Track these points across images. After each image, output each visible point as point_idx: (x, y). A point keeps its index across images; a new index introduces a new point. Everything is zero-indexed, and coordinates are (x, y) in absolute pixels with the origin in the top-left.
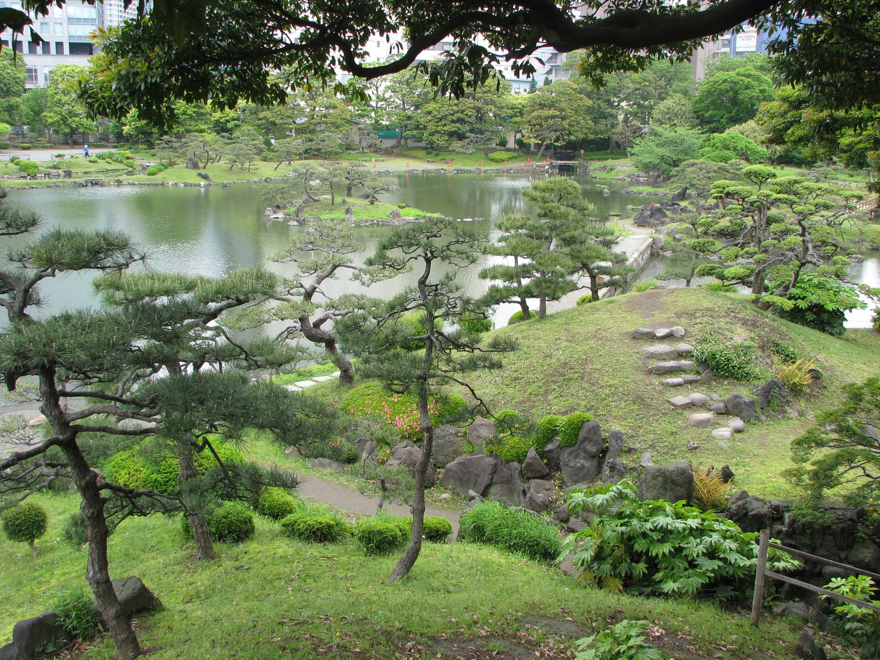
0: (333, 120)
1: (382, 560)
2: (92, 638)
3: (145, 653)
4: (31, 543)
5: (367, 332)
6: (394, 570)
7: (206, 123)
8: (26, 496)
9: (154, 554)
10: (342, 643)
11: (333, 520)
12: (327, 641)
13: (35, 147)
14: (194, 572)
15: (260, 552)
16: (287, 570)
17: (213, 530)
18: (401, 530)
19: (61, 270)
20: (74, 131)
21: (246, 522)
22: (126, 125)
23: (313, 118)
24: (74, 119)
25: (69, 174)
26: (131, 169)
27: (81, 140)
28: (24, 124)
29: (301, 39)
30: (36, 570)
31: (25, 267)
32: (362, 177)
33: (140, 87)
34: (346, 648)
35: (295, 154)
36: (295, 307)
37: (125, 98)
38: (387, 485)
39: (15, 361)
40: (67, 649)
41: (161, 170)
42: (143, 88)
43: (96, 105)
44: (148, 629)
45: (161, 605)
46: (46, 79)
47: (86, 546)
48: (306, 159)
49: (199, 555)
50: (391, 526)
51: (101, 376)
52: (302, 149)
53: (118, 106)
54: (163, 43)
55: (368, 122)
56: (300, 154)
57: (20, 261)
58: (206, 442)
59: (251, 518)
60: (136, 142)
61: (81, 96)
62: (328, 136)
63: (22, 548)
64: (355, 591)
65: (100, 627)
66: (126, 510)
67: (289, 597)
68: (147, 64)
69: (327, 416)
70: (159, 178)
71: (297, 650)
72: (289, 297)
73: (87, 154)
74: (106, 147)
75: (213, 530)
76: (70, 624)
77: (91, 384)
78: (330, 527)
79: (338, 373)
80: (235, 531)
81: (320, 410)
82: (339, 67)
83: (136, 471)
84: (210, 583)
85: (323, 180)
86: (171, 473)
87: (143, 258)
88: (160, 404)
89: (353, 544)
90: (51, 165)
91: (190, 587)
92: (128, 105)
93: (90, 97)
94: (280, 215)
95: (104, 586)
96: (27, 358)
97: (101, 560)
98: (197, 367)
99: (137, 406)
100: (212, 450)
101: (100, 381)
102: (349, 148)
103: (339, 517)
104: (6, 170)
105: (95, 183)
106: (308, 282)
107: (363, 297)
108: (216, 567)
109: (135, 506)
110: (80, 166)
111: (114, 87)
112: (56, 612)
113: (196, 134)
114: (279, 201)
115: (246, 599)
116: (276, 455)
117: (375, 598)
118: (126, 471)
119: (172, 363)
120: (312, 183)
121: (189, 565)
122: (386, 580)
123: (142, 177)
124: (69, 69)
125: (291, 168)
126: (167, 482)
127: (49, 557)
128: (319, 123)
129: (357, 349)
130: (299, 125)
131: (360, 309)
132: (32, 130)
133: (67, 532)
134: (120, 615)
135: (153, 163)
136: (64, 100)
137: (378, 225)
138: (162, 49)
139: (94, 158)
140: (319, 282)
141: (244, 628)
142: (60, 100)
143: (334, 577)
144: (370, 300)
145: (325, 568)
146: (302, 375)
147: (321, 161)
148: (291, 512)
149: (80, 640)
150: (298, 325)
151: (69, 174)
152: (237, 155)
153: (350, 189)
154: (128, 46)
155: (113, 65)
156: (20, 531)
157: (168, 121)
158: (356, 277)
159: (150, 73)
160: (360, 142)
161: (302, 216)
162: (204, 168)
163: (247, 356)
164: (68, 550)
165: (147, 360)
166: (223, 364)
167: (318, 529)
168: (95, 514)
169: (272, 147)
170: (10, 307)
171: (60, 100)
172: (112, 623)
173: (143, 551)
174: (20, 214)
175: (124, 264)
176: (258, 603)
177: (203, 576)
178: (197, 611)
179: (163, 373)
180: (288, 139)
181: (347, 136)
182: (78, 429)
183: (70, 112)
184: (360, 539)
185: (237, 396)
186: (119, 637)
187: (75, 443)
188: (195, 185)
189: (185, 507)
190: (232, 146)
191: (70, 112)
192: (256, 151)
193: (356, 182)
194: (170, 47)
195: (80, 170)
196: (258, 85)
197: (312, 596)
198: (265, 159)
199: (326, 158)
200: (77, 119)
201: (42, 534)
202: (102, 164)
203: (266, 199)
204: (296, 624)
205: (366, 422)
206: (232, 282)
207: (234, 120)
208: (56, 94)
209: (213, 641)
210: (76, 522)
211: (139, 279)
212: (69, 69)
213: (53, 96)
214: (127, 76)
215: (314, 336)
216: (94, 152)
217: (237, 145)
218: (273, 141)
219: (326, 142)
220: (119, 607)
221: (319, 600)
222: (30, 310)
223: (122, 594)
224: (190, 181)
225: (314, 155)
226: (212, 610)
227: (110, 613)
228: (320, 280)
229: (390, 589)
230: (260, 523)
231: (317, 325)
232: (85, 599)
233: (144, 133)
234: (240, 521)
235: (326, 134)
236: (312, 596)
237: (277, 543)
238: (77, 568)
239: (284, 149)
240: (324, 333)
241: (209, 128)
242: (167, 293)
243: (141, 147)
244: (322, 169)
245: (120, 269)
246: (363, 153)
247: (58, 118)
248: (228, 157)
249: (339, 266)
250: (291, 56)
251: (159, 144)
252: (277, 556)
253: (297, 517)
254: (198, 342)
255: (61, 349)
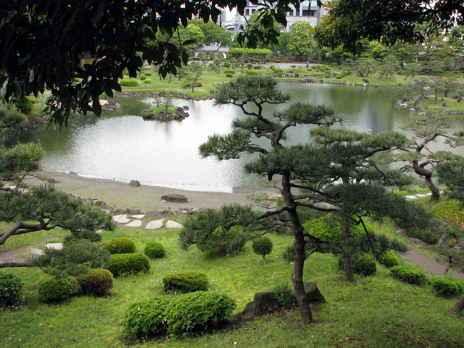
0: (440, 54)
1: (445, 301)
2: (289, 309)
3: (315, 322)
4: (264, 257)
5: (455, 173)
6: (453, 308)
7: (369, 53)
8: (265, 233)
9: (322, 273)
10: (420, 342)
11: (420, 273)
12: (412, 338)
13: (282, 62)
14: (342, 286)
15: (378, 283)
16: (391, 295)
17: (354, 267)
18: (459, 286)
19: (299, 123)
20: (301, 54)
21: (372, 266)
22: (327, 52)
23: (429, 52)
24: (302, 48)
25: (297, 76)
26: (328, 75)
27: (304, 59)
28: (278, 50)
29: (435, 7)
30: (265, 270)
31: (281, 120)
32: (454, 86)
33: (347, 32)
34: (423, 345)
35: (417, 72)
36: (411, 155)
37: (338, 38)
38: (453, 260)
39: (274, 166)
40: (278, 311)
41: (343, 76)
42: (348, 33)
43: (323, 41)
44: (316, 310)
45: (324, 300)
46: (290, 28)
47: (292, 263)
48: (422, 74)
49: (346, 278)
50: (453, 283)
51: (311, 179)
52: (421, 69)
53: (334, 42)
54: (361, 9)
55: (461, 55)
56: (419, 72)
57: (279, 117)
58: (361, 220)
59: (375, 264)
60: (332, 61)
61: (316, 36)
62: (436, 63)
63: (260, 258)
64: (429, 315)
65: (294, 304)
66: (314, 249)
67: (391, 310)
68: (351, 21)
69: (425, 216)
70: (342, 80)
71: (396, 340)
72: (408, 149)
73: (307, 66)
74: (316, 63)
75: (354, 267)
76: (280, 299)
77: (306, 182)
78: (417, 276)
79: (430, 194)
80: (366, 269)
81: (421, 212)
82: (456, 22)
83: (318, 230)
84: (350, 294)
85: (432, 87)
86: (336, 233)
87: (340, 121)
88: (341, 197)
89: (429, 289)
90: (289, 71)
91: (339, 294)
92: (340, 41)
93: (320, 37)
94: (405, 105)
95: (299, 284)
96: (280, 165)
97: (300, 270)
98: (358, 180)
99: (328, 197)
100: (364, 225)
101: (311, 181)
102: (448, 69)
103: (423, 272)
104: (268, 72)
105: (310, 81)
106: (420, 142)
107: (450, 153)
108: (353, 286)
109: (319, 247)
110: (303, 72)
111: (333, 32)
112: (274, 292)
113: (364, 58)
114: (406, 97)
115: (368, 306)
116: (391, 233)
117: (440, 321)
118: (313, 229)
119: (345, 177)
120: (425, 88)
121: (340, 282)
122: (448, 313)
123: (334, 79)
124: (302, 23)
125: (414, 79)
126: (333, 238)
127: (271, 264)
128: (432, 55)
129: (448, 181)
130: (421, 56)
131: (448, 160)
132: (282, 53)
133: (285, 254)
134: (305, 300)
135: (339, 73)
136: (298, 39)
137: (461, 114)
138: (360, 13)
139: (310, 68)
140: (426, 143)
141: (367, 321)
142: (296, 39)
143: (417, 304)
144: (454, 155)
145: (413, 299)
146: (411, 192)
147: (431, 76)
148: (396, 264)
149: (284, 308)
150: (412, 165)
151: (297, 76)
152: (384, 71)
153: (447, 92)
154: (342, 10)
155: (334, 21)
156: (260, 249)
157: (358, 50)
158: (448, 142)
159: (353, 25)
160: (455, 66)
161: (418, 106)
162: (366, 76)
163: (385, 178)
164: (282, 262)
165: (335, 174)
166: (371, 181)
167: (411, 277)
168: (301, 248)
169: (404, 68)
170: (273, 140)
171: (296, 39)
172: (301, 304)
173: (317, 271)
174: (282, 93)
175: (331, 123)
176: (375, 310)
177: (346, 289)
178: (342, 307)
179: (339, 182)
180: (413, 63)
181: (447, 63)
182: (298, 204)
183: (300, 45)
184: (434, 286)
185: (382, 199)
186: (303, 311)
187: (296, 211)
188: (361, 85)
189: (344, 252)
190: (382, 65)
191: (300, 45)
192: (395, 69)
193: (450, 89)
194: (364, 12)
195: (303, 74)
196: (408, 32)
197: (404, 312)
198: (399, 74)
199: (434, 75)
200: (303, 48)
201: (269, 253)
202: (314, 72)
203: (399, 95)
204: (395, 325)
205: (445, 223)
206: (382, 138)
207: (384, 51)
208: (294, 35)
209: (350, 324)
210: (290, 250)
211: (334, 131)
212: (302, 23)
213: (293, 36)
214: (341, 26)
215: (420, 170)
216: (311, 65)
217: (385, 65)
218: (404, 64)
219: (435, 66)
220: (305, 296)
221: (408, 315)
222: (281, 142)
223: (307, 290)
224: (358, 83)
225: (427, 73)
226: (350, 308)
227: (300, 298)
228: (427, 142)
229: (449, 318)
230: (380, 268)
231: (422, 166)
232: (288, 289)
233: (336, 57)
234: (369, 265)
235: (436, 61)
236: (404, 312)
237: (387, 280)
238: (284, 273)
239: (411, 69)
240: (425, 171)
241: (370, 56)
242: (347, 140)
243: (334, 64)
244: (431, 81)
245: (328, 126)
246: (456, 73)
247: (294, 47)
248: (379, 71)
249: (438, 135)
250: (428, 17)
251: (343, 63)
252: (386, 287)
253: (400, 268)
254: (360, 167)
255: (297, 163)
